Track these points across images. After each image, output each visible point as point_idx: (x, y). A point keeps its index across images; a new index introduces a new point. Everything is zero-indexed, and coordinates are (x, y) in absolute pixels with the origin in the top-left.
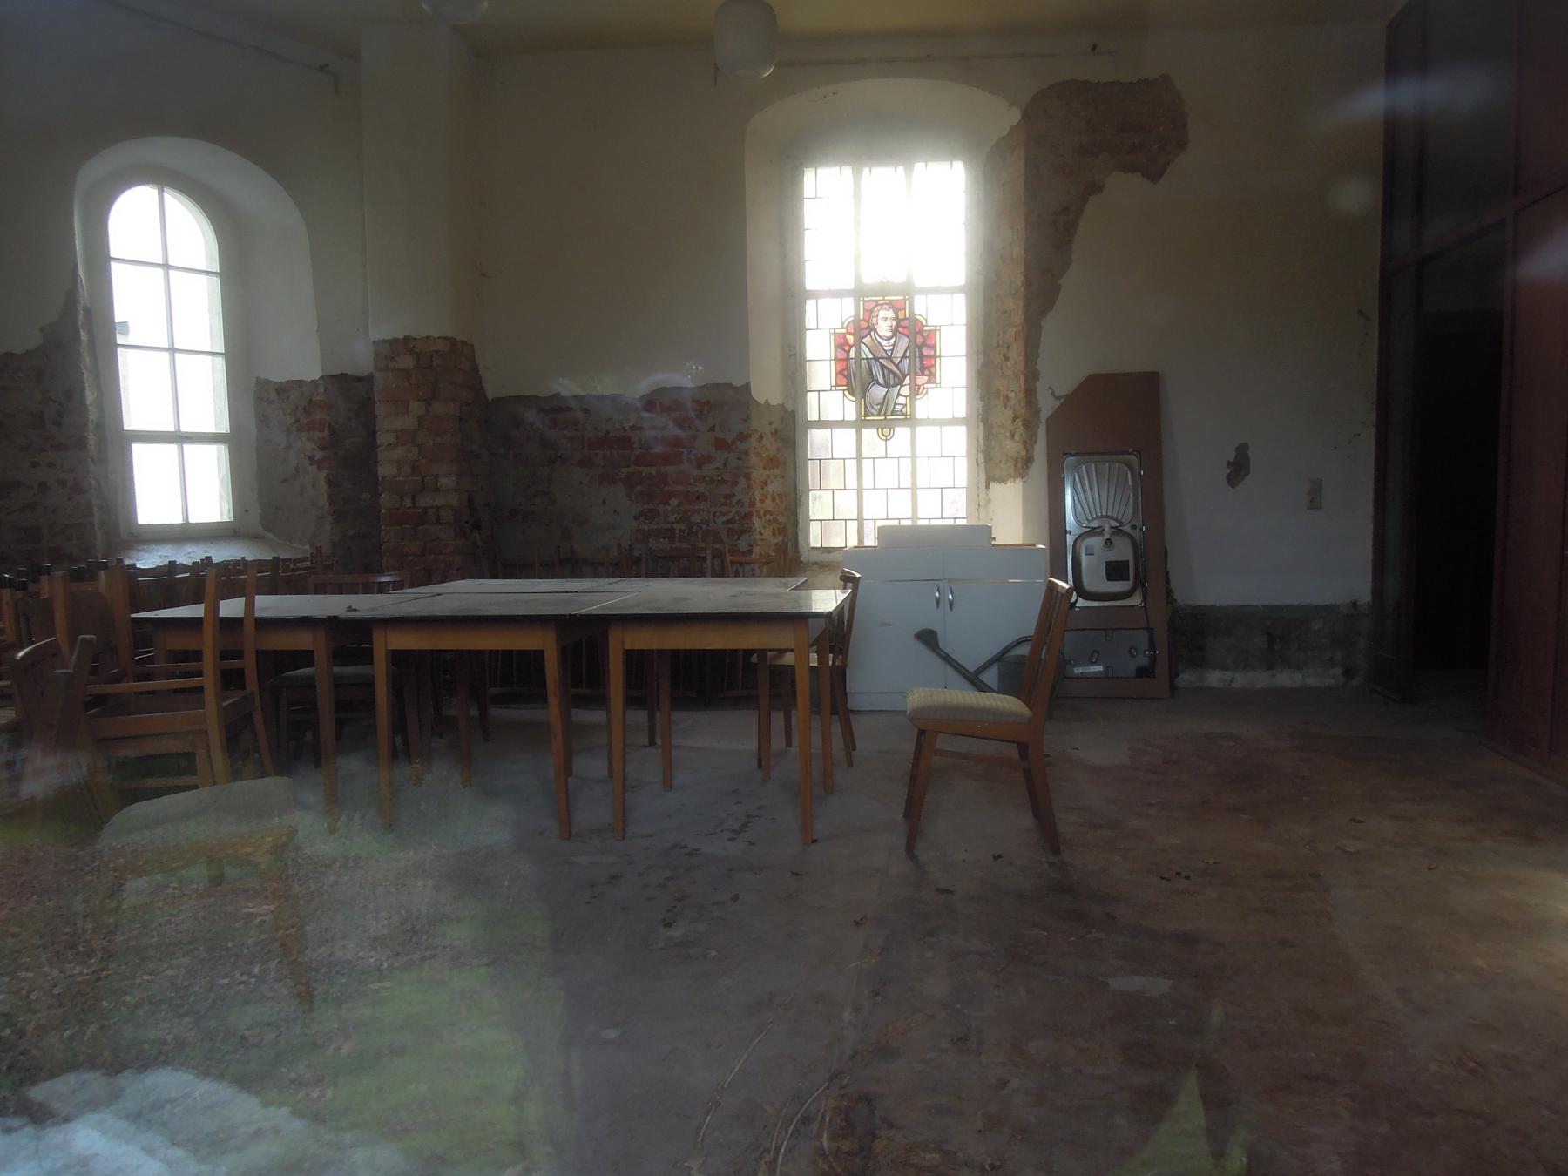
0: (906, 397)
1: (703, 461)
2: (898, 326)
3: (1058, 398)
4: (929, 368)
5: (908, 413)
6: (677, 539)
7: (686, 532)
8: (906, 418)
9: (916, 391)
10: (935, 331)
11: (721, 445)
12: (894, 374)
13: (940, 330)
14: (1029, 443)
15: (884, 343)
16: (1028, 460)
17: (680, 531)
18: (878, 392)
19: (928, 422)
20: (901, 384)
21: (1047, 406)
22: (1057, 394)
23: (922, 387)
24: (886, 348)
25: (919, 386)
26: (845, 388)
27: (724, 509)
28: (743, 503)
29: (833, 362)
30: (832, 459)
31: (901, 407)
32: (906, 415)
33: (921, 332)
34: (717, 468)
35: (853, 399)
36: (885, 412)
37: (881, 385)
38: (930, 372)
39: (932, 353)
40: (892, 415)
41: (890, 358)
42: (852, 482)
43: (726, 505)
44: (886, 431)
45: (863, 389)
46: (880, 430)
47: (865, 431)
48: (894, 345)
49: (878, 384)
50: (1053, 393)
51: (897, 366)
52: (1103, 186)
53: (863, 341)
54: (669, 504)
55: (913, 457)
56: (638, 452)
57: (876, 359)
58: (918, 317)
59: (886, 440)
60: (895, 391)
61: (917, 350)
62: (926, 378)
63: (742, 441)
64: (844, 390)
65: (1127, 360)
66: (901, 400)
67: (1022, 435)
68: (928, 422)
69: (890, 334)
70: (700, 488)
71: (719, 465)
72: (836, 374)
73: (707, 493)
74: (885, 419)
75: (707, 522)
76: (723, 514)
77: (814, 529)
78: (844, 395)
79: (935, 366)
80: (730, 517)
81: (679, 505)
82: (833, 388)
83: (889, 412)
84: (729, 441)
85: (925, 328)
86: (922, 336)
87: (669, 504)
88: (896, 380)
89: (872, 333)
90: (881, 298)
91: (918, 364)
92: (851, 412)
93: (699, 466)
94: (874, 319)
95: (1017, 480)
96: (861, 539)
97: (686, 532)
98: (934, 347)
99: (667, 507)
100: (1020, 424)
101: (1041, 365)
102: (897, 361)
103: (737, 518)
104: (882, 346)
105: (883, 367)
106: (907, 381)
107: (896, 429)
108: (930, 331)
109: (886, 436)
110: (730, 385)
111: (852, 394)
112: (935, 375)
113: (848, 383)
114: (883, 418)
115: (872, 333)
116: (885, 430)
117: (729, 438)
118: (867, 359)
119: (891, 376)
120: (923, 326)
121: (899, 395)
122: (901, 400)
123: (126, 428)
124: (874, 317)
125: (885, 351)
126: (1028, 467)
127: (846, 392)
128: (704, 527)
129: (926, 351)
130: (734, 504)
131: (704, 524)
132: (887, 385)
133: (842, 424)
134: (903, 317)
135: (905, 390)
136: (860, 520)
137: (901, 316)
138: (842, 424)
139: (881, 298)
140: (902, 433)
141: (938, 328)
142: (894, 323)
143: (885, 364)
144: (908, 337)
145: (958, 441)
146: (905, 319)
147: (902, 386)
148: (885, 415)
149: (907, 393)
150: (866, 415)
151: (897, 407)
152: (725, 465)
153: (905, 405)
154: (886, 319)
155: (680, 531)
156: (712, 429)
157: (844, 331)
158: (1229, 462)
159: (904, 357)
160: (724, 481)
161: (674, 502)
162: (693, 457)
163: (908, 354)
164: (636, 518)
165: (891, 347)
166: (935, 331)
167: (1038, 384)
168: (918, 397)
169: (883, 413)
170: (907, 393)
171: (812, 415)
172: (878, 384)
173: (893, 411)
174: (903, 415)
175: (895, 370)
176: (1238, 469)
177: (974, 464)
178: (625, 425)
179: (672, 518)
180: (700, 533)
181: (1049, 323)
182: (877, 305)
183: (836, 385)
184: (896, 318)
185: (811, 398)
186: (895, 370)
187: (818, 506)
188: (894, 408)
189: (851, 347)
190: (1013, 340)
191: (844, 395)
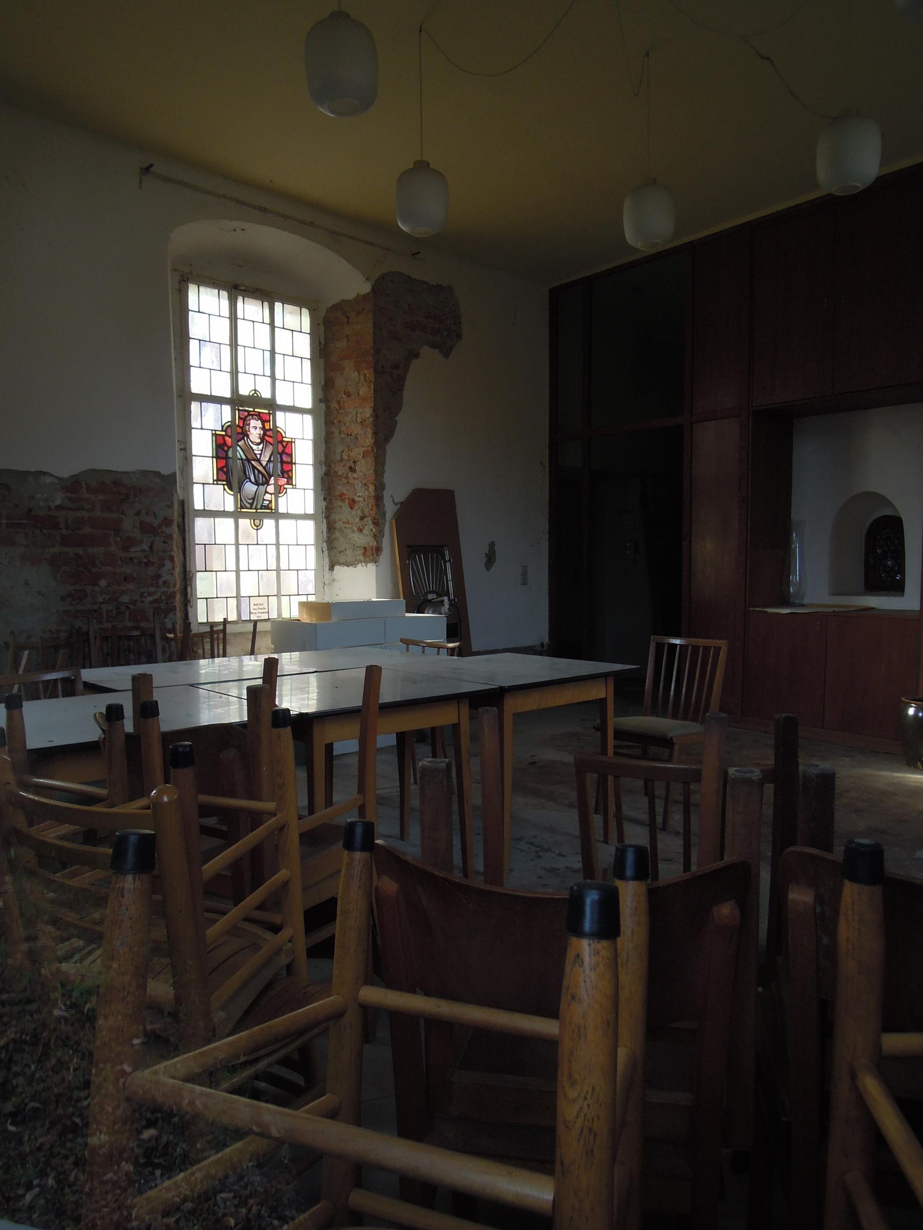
0: (271, 494)
1: (128, 544)
2: (265, 434)
3: (396, 504)
4: (287, 472)
5: (273, 508)
6: (104, 620)
7: (114, 612)
8: (271, 512)
9: (279, 490)
10: (292, 442)
11: (147, 529)
12: (263, 475)
13: (294, 442)
14: (378, 537)
15: (254, 447)
16: (378, 550)
17: (108, 611)
18: (250, 488)
19: (287, 516)
20: (267, 483)
21: (390, 509)
22: (396, 501)
23: (282, 488)
24: (256, 452)
25: (281, 486)
26: (225, 483)
27: (152, 589)
28: (169, 584)
29: (215, 459)
30: (215, 544)
31: (268, 502)
32: (272, 509)
33: (282, 441)
34: (144, 551)
35: (232, 493)
36: (256, 507)
37: (252, 483)
38: (288, 475)
39: (290, 460)
40: (261, 509)
41: (259, 461)
42: (232, 566)
43: (153, 586)
44: (257, 522)
45: (239, 484)
46: (252, 521)
47: (241, 521)
48: (262, 450)
49: (250, 481)
50: (393, 500)
51: (264, 468)
52: (420, 353)
53: (240, 443)
54: (97, 585)
55: (278, 545)
56: (64, 532)
57: (249, 460)
58: (279, 429)
59: (257, 530)
60: (262, 488)
61: (279, 456)
62: (286, 480)
63: (167, 527)
64: (224, 485)
65: (433, 480)
66: (268, 497)
67: (372, 530)
68: (287, 516)
69: (259, 441)
70: (128, 570)
71: (145, 547)
72: (218, 470)
73: (135, 575)
74: (256, 512)
75: (134, 602)
76: (150, 594)
77: (201, 606)
78: (224, 489)
79: (291, 470)
80: (157, 596)
81: (109, 585)
82: (215, 482)
83: (259, 507)
84: (155, 525)
85: (284, 439)
86: (282, 445)
87: (97, 585)
88: (264, 479)
89: (246, 438)
90: (252, 409)
91: (279, 469)
92: (230, 506)
93: (126, 549)
94: (247, 427)
95: (370, 565)
96: (279, 614)
97: (114, 612)
98: (291, 455)
99: (96, 588)
100: (370, 522)
101: (387, 478)
102: (264, 463)
103: (163, 598)
104: (253, 450)
105: (254, 468)
106: (272, 481)
107: (264, 520)
108: (288, 442)
109: (257, 526)
110: (158, 474)
111: (231, 489)
112: (291, 478)
113: (227, 478)
114: (254, 511)
115: (246, 438)
116: (256, 521)
117: (156, 523)
118: (242, 459)
119: (260, 476)
120: (283, 437)
121: (266, 492)
122: (268, 497)
123: (274, 520)
124: (247, 425)
125: (255, 454)
126: (378, 555)
127: (226, 487)
128: (131, 606)
129: (285, 458)
130: (160, 584)
131: (131, 603)
132: (257, 483)
133: (223, 514)
134: (268, 428)
135: (271, 489)
136: (238, 597)
137: (267, 427)
138: (223, 514)
139: (252, 409)
140: (269, 523)
141: (293, 440)
142: (262, 432)
143: (256, 465)
144: (271, 444)
145: (308, 531)
146: (270, 430)
147: (268, 485)
148: (256, 509)
149: (272, 491)
150: (242, 508)
151: (265, 502)
152: (151, 547)
153: (271, 502)
154: (256, 428)
155: (108, 611)
156: (138, 514)
157: (224, 433)
158: (486, 554)
159: (269, 461)
160: (148, 564)
161: (103, 583)
162: (118, 539)
163: (272, 459)
164: (63, 599)
165: (260, 452)
166: (292, 442)
167: (385, 493)
168: (280, 495)
169: (254, 507)
170: (272, 491)
171: (198, 505)
172: (250, 481)
173: (262, 505)
174: (269, 509)
175: (264, 472)
176: (490, 559)
177: (320, 552)
178: (51, 504)
179: (100, 600)
180: (127, 612)
181: (392, 448)
182: (249, 415)
183: (218, 480)
184: (263, 428)
185: (197, 490)
186: (264, 472)
187: (203, 585)
188: (263, 503)
189: (229, 448)
190: (360, 456)
191: (224, 489)
